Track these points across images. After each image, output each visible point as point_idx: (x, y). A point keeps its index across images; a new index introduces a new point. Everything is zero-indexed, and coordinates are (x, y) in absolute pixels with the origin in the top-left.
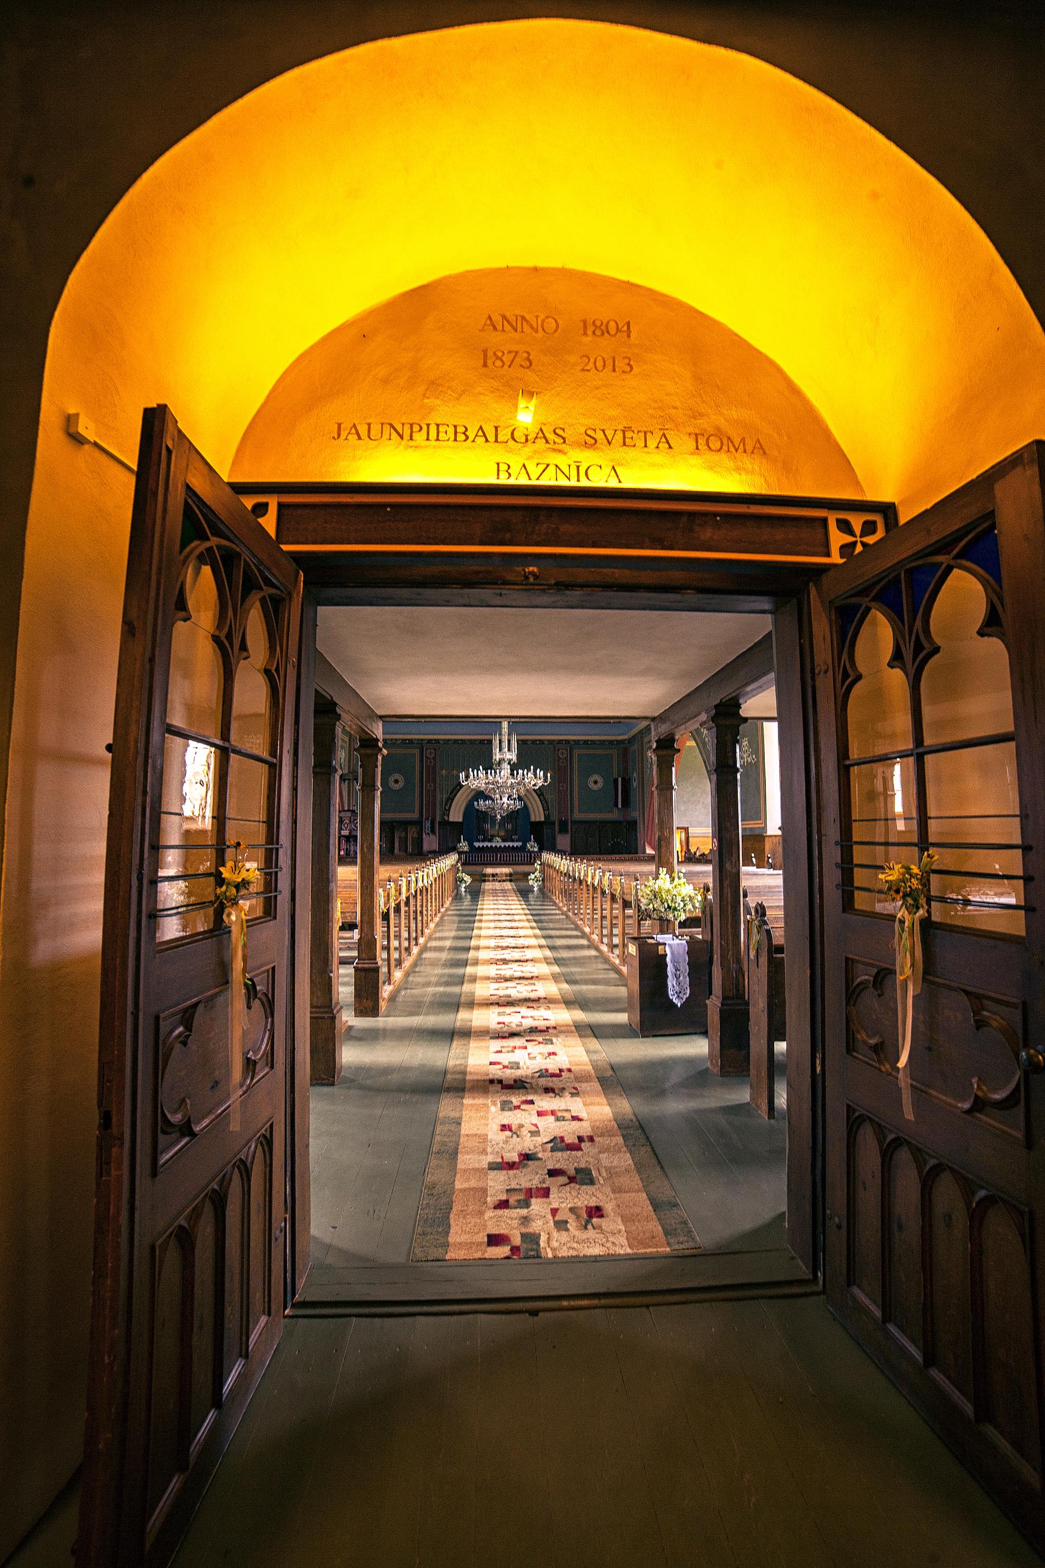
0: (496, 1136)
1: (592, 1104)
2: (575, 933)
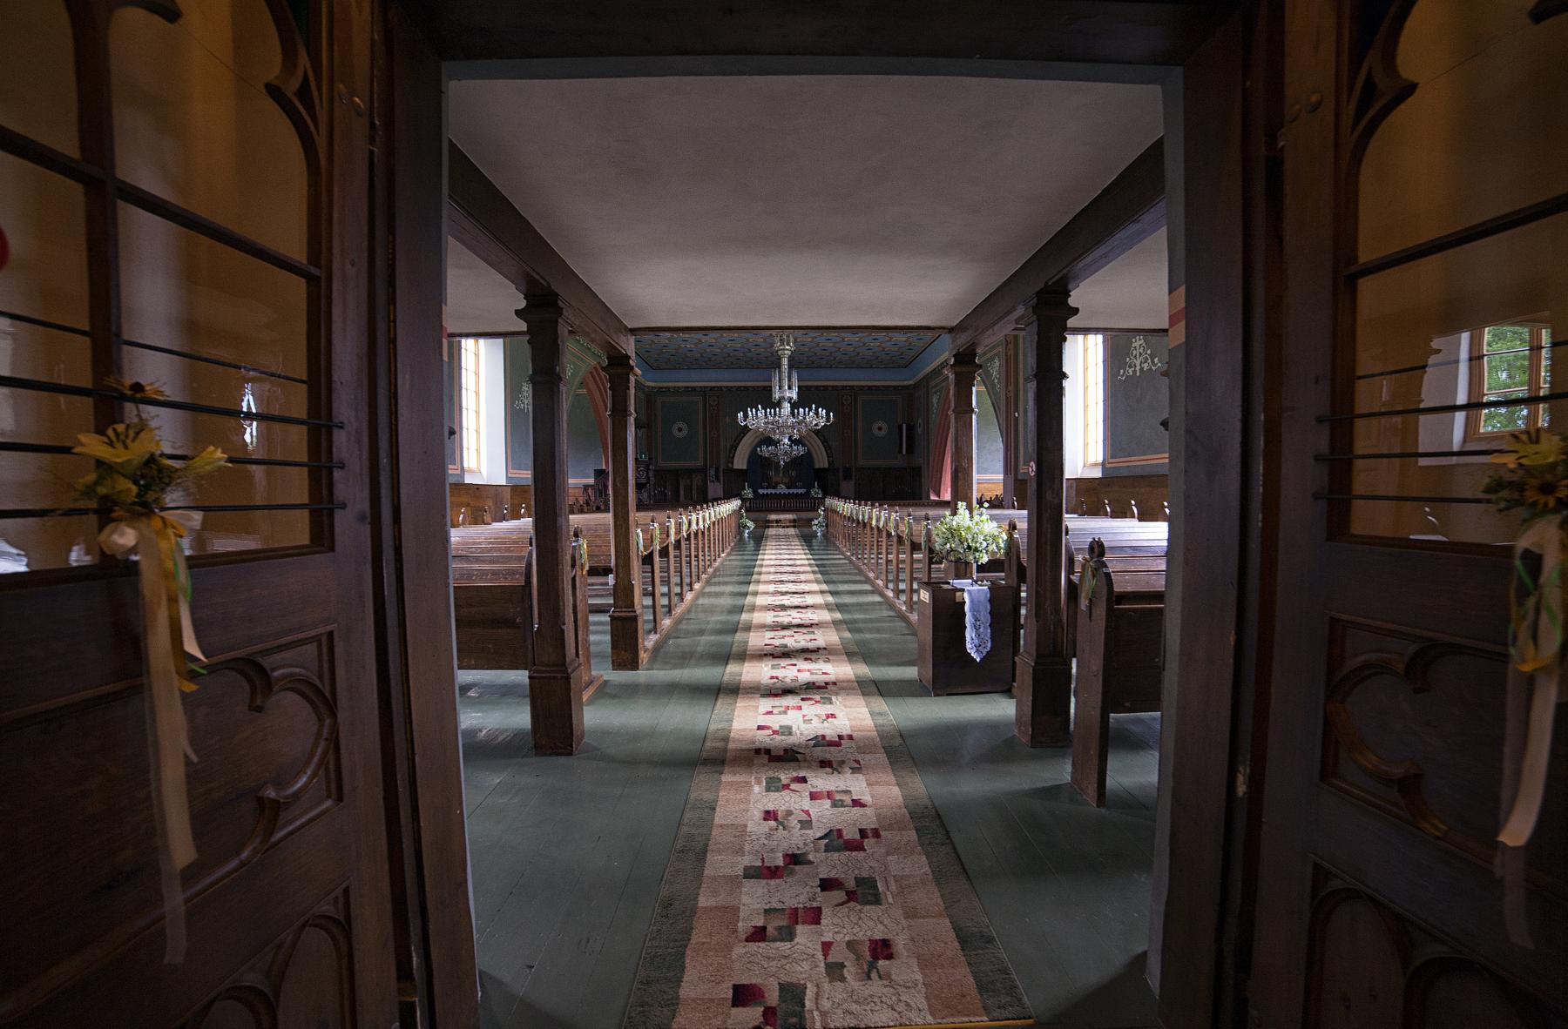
0: (757, 826)
1: (877, 783)
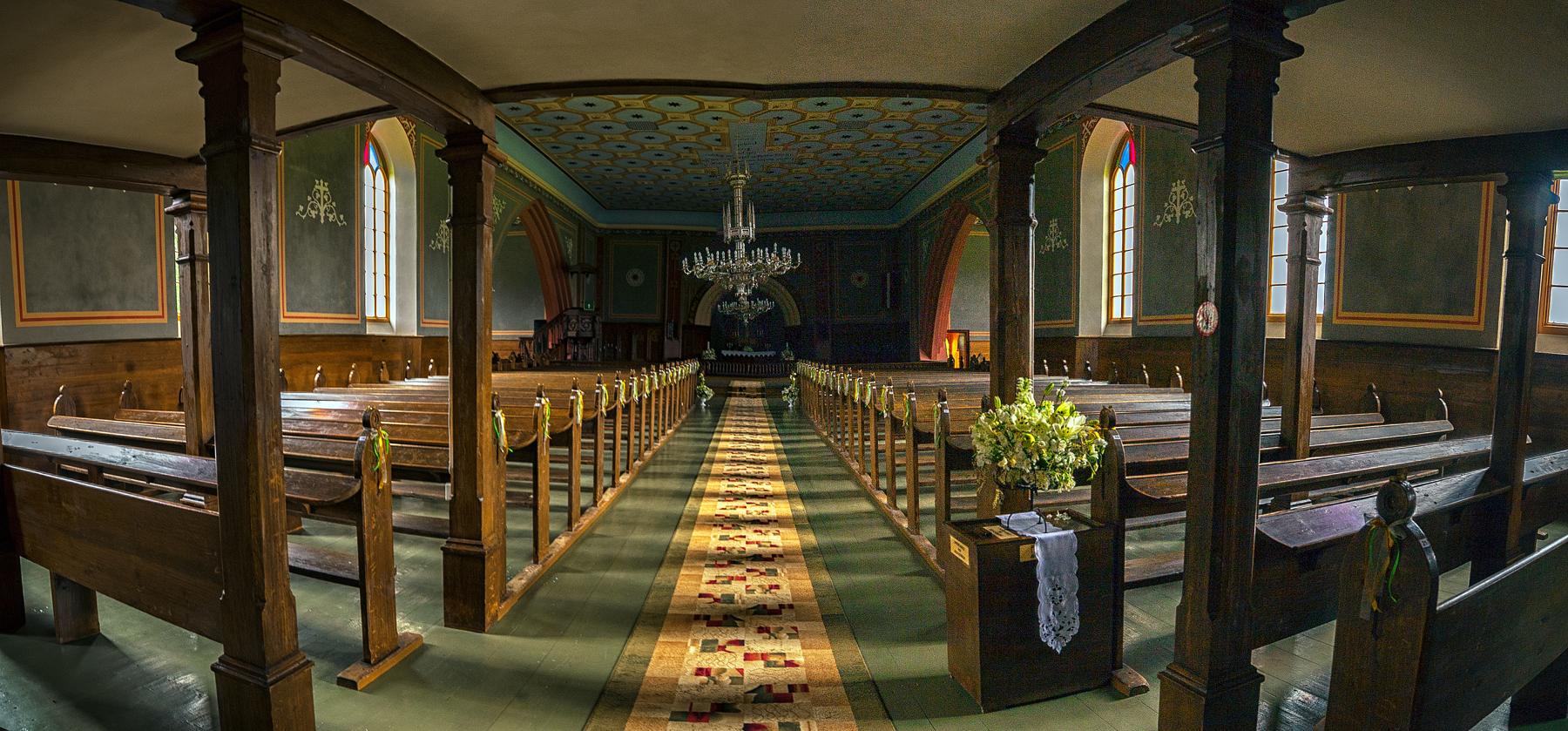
2: (838, 470)
